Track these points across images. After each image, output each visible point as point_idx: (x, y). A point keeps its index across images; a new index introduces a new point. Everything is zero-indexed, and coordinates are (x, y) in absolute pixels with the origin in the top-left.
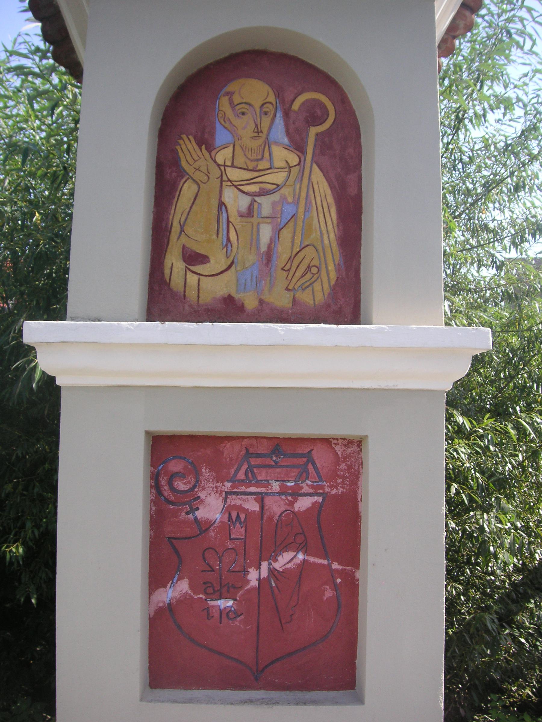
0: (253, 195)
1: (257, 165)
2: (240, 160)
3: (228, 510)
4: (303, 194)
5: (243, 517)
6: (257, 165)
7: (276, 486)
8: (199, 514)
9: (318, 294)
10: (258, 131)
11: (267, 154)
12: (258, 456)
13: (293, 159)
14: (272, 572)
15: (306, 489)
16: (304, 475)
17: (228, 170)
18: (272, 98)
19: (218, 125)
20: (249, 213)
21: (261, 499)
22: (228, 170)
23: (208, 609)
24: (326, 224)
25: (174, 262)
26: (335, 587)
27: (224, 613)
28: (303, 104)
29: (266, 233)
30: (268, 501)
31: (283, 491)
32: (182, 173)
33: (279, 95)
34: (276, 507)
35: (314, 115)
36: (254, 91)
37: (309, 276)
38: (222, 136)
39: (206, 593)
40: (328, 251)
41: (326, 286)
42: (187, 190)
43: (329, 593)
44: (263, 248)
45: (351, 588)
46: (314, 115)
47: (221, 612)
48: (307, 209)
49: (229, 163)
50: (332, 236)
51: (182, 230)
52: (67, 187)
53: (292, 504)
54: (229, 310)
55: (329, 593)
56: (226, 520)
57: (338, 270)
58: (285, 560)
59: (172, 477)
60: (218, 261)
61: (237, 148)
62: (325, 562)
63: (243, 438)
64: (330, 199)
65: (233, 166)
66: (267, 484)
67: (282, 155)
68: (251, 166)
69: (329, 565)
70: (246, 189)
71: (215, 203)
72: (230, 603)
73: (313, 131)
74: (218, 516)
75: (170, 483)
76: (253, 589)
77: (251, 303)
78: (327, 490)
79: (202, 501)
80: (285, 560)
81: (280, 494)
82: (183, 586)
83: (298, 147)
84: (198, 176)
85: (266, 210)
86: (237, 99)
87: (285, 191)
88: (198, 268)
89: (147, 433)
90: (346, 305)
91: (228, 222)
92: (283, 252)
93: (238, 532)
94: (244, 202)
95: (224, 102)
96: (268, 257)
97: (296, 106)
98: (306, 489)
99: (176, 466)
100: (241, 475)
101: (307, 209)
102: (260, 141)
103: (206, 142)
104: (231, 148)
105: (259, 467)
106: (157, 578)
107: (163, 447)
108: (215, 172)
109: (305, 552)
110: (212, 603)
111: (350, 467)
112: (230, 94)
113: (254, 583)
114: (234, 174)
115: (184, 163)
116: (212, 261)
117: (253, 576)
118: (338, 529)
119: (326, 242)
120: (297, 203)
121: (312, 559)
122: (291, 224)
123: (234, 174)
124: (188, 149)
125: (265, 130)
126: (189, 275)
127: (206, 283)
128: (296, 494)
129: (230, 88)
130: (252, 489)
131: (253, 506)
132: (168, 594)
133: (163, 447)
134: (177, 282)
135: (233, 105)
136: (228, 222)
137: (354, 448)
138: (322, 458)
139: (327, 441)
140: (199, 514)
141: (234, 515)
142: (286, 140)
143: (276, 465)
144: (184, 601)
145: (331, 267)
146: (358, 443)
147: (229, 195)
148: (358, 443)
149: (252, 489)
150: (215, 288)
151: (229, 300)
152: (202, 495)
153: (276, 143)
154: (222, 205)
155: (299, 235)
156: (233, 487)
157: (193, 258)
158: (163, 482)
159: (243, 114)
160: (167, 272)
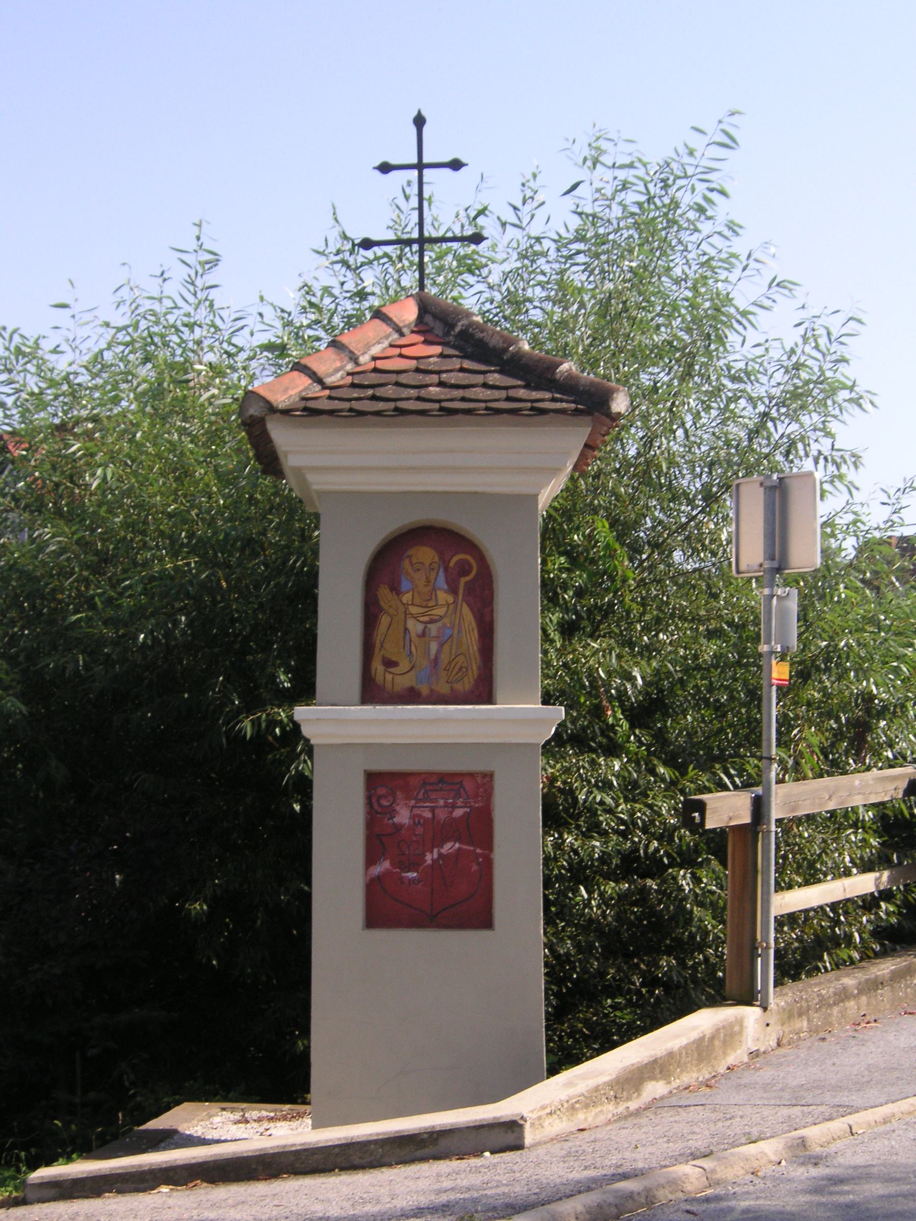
0: (425, 623)
1: (429, 608)
2: (417, 600)
3: (413, 817)
4: (457, 622)
5: (422, 821)
6: (429, 608)
7: (441, 802)
8: (396, 820)
9: (466, 685)
10: (428, 581)
11: (434, 597)
12: (432, 784)
13: (451, 599)
14: (440, 855)
15: (459, 804)
16: (458, 795)
17: (410, 607)
18: (437, 559)
19: (403, 578)
20: (423, 634)
21: (433, 809)
22: (410, 607)
23: (402, 878)
24: (471, 639)
25: (377, 666)
26: (478, 864)
27: (412, 881)
28: (456, 563)
29: (434, 647)
30: (437, 811)
31: (446, 805)
32: (381, 610)
33: (441, 555)
34: (442, 815)
35: (464, 569)
36: (425, 554)
37: (461, 673)
38: (405, 585)
39: (400, 868)
40: (473, 658)
41: (471, 680)
42: (384, 620)
43: (475, 868)
44: (432, 657)
45: (487, 866)
46: (464, 569)
47: (410, 880)
48: (459, 631)
49: (410, 603)
50: (475, 648)
51: (382, 646)
52: (695, 908)
53: (451, 813)
54: (411, 697)
55: (475, 868)
56: (412, 823)
57: (479, 668)
58: (448, 847)
59: (379, 798)
60: (404, 666)
61: (415, 593)
62: (472, 848)
63: (422, 774)
64: (474, 624)
65: (412, 604)
66: (435, 801)
67: (443, 597)
68: (424, 604)
69: (474, 851)
70: (422, 619)
71: (402, 628)
72: (415, 874)
73: (463, 580)
74: (407, 821)
75: (378, 801)
76: (428, 865)
77: (425, 691)
78: (473, 804)
79: (397, 812)
80: (448, 847)
81: (444, 807)
82: (386, 864)
83: (453, 590)
84: (391, 611)
85: (434, 633)
86: (414, 561)
87: (445, 620)
88: (392, 670)
89: (365, 771)
90: (483, 692)
91: (411, 641)
92: (444, 658)
93: (420, 830)
94: (420, 627)
95: (406, 564)
96: (436, 661)
97: (452, 564)
98: (459, 804)
99: (382, 791)
100: (420, 796)
101: (459, 631)
102: (430, 588)
103: (395, 589)
104: (411, 593)
105: (432, 790)
106: (371, 859)
107: (373, 779)
108: (402, 609)
109: (460, 843)
110: (404, 875)
111: (486, 791)
112: (410, 557)
113: (429, 862)
114: (414, 610)
115: (382, 603)
116: (401, 665)
117: (429, 858)
118: (479, 828)
119: (471, 652)
120: (453, 627)
121: (465, 847)
122: (450, 640)
123: (414, 610)
124: (384, 593)
125: (433, 581)
126: (387, 674)
127: (398, 679)
128: (454, 806)
129: (410, 552)
130: (427, 804)
131: (428, 814)
132: (377, 870)
133: (373, 779)
134: (379, 678)
135: (411, 563)
136: (411, 641)
137: (487, 779)
138: (468, 785)
139: (471, 775)
140: (396, 820)
141: (417, 820)
142: (446, 587)
143: (441, 790)
144: (386, 874)
145: (475, 667)
146: (489, 776)
147: (411, 623)
148: (489, 776)
149: (427, 804)
150: (403, 682)
151: (412, 689)
152: (397, 808)
153: (439, 589)
154: (406, 630)
155: (454, 647)
156: (416, 803)
157: (389, 664)
158: (374, 800)
159: (418, 570)
160: (373, 672)
